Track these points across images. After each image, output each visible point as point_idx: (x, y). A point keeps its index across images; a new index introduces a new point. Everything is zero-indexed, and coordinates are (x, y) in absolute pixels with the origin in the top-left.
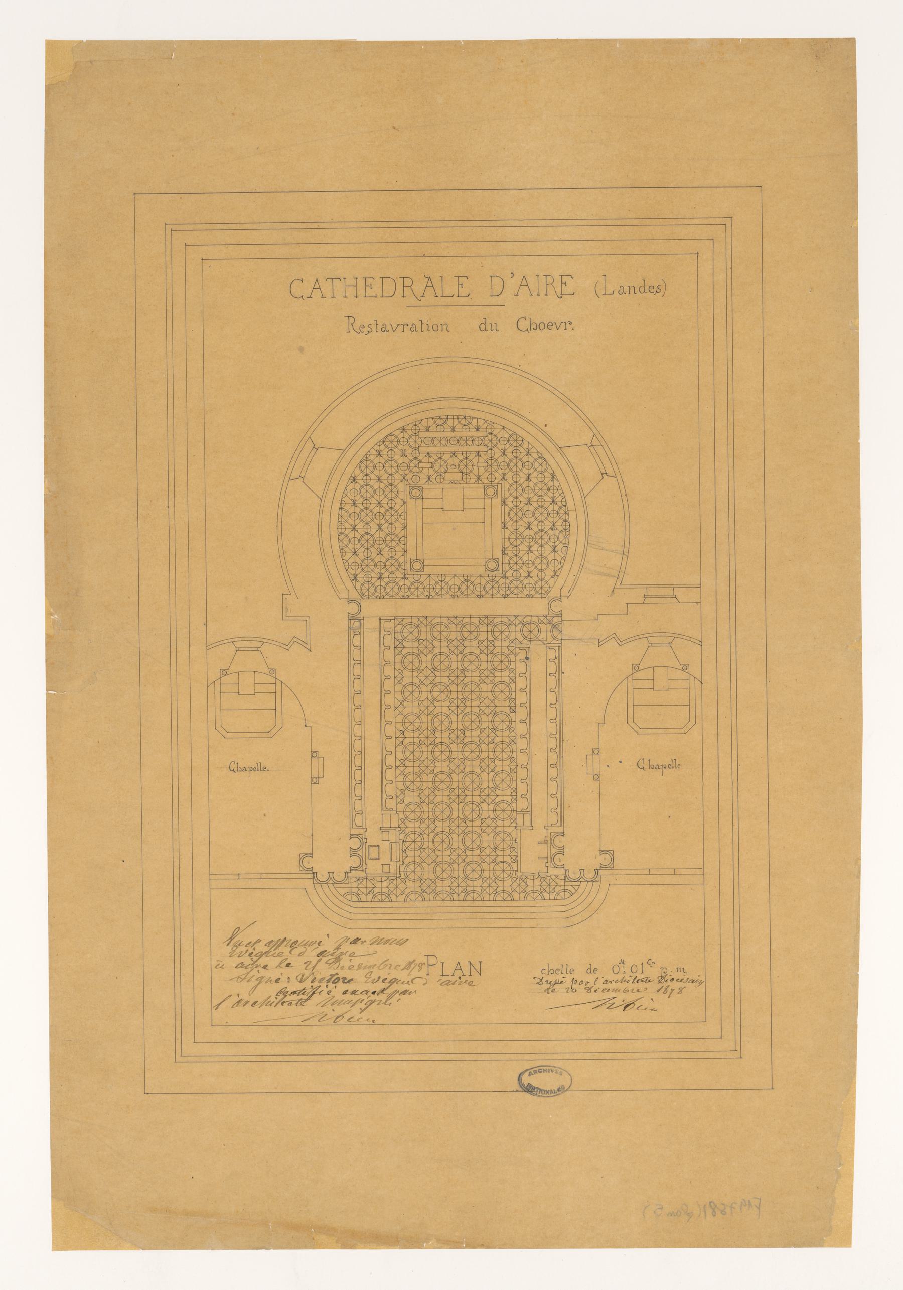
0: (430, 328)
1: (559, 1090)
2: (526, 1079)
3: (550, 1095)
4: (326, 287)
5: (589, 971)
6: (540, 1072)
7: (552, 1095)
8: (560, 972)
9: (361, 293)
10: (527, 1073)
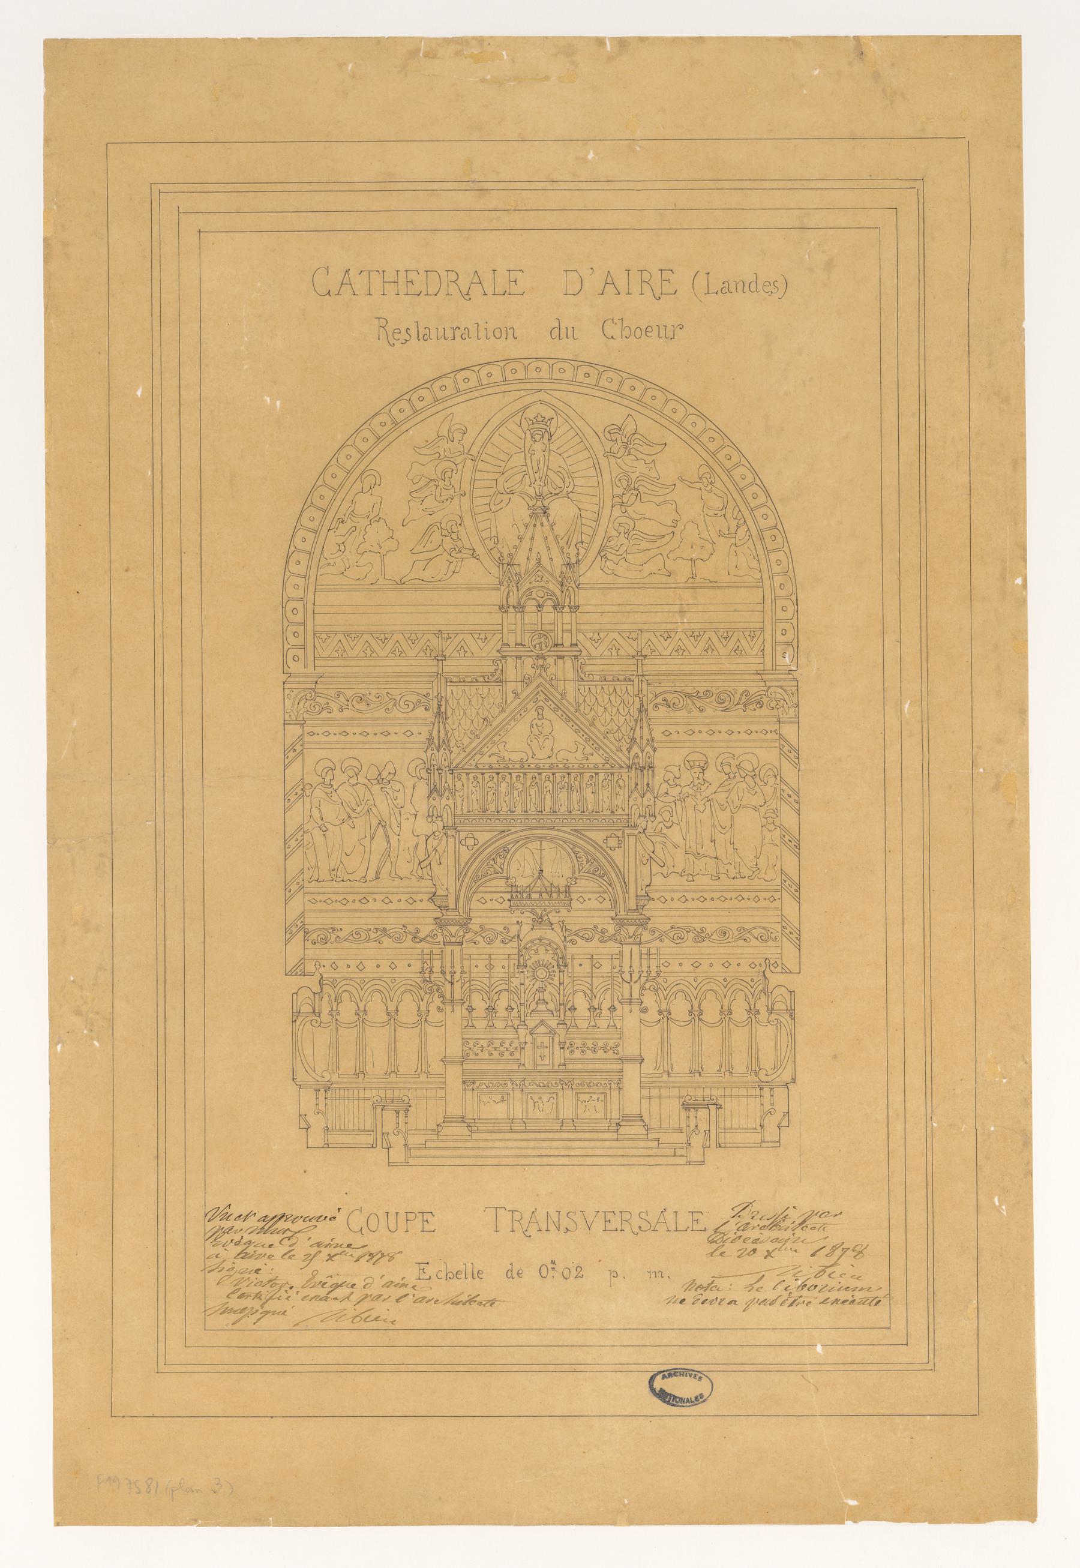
0: (490, 334)
1: (696, 1398)
2: (658, 1384)
3: (685, 1405)
4: (359, 283)
5: (509, 1274)
6: (676, 1376)
7: (688, 1404)
8: (463, 1276)
9: (403, 289)
10: (660, 1376)
